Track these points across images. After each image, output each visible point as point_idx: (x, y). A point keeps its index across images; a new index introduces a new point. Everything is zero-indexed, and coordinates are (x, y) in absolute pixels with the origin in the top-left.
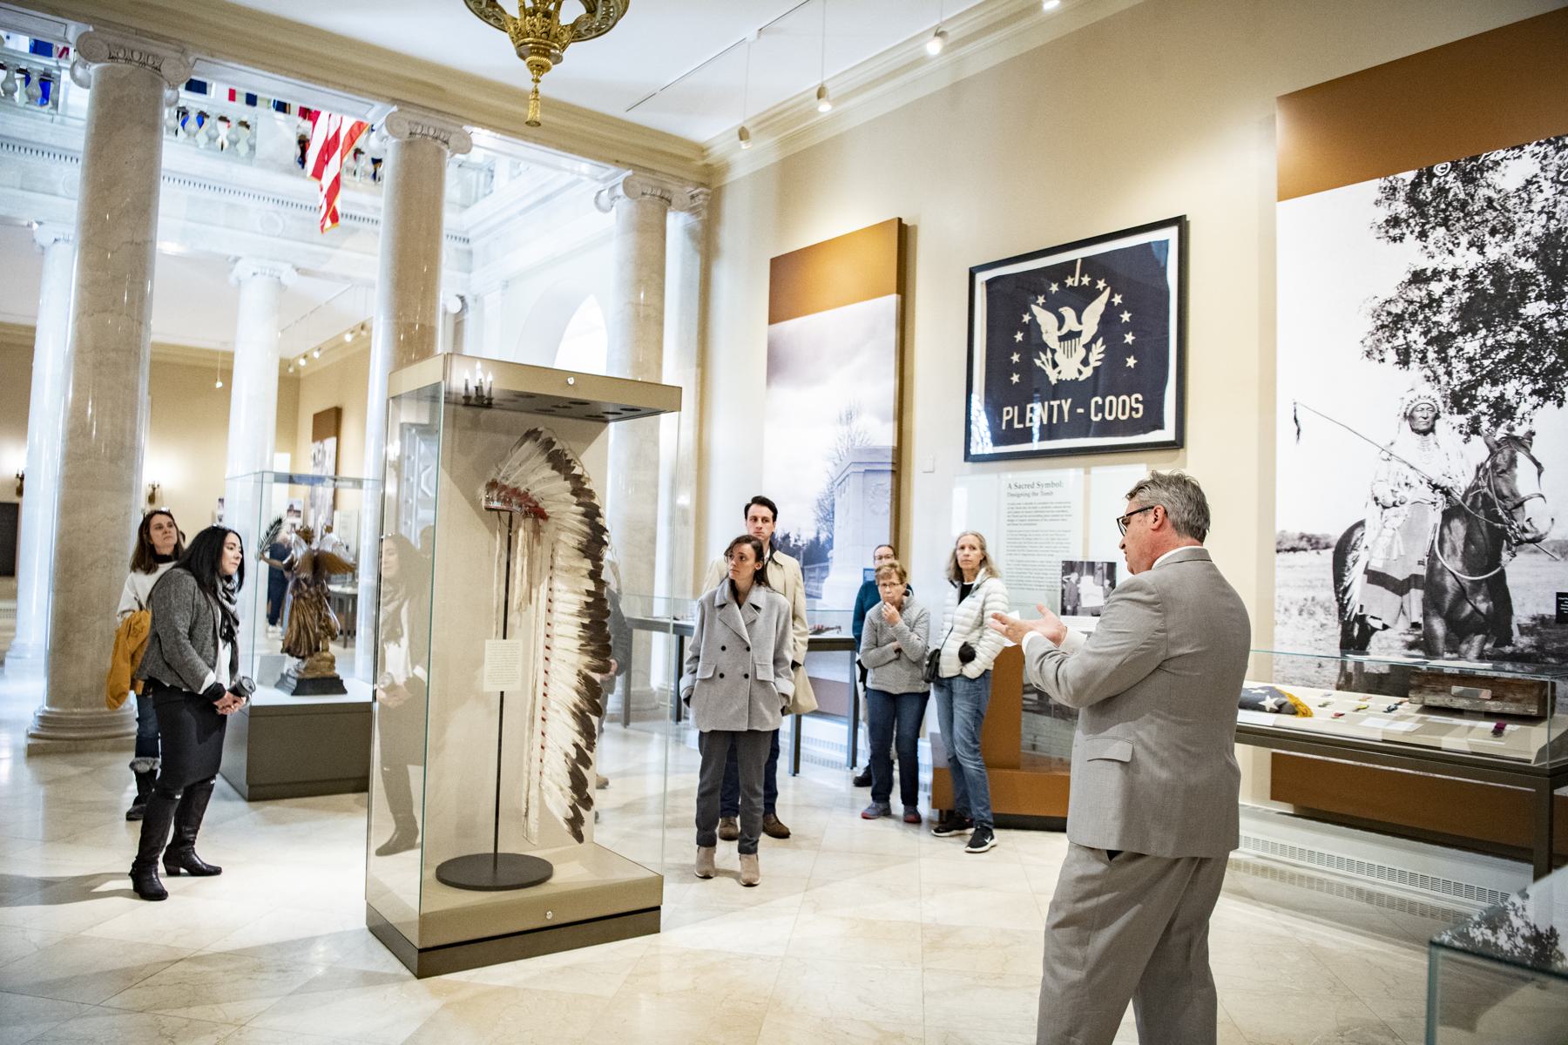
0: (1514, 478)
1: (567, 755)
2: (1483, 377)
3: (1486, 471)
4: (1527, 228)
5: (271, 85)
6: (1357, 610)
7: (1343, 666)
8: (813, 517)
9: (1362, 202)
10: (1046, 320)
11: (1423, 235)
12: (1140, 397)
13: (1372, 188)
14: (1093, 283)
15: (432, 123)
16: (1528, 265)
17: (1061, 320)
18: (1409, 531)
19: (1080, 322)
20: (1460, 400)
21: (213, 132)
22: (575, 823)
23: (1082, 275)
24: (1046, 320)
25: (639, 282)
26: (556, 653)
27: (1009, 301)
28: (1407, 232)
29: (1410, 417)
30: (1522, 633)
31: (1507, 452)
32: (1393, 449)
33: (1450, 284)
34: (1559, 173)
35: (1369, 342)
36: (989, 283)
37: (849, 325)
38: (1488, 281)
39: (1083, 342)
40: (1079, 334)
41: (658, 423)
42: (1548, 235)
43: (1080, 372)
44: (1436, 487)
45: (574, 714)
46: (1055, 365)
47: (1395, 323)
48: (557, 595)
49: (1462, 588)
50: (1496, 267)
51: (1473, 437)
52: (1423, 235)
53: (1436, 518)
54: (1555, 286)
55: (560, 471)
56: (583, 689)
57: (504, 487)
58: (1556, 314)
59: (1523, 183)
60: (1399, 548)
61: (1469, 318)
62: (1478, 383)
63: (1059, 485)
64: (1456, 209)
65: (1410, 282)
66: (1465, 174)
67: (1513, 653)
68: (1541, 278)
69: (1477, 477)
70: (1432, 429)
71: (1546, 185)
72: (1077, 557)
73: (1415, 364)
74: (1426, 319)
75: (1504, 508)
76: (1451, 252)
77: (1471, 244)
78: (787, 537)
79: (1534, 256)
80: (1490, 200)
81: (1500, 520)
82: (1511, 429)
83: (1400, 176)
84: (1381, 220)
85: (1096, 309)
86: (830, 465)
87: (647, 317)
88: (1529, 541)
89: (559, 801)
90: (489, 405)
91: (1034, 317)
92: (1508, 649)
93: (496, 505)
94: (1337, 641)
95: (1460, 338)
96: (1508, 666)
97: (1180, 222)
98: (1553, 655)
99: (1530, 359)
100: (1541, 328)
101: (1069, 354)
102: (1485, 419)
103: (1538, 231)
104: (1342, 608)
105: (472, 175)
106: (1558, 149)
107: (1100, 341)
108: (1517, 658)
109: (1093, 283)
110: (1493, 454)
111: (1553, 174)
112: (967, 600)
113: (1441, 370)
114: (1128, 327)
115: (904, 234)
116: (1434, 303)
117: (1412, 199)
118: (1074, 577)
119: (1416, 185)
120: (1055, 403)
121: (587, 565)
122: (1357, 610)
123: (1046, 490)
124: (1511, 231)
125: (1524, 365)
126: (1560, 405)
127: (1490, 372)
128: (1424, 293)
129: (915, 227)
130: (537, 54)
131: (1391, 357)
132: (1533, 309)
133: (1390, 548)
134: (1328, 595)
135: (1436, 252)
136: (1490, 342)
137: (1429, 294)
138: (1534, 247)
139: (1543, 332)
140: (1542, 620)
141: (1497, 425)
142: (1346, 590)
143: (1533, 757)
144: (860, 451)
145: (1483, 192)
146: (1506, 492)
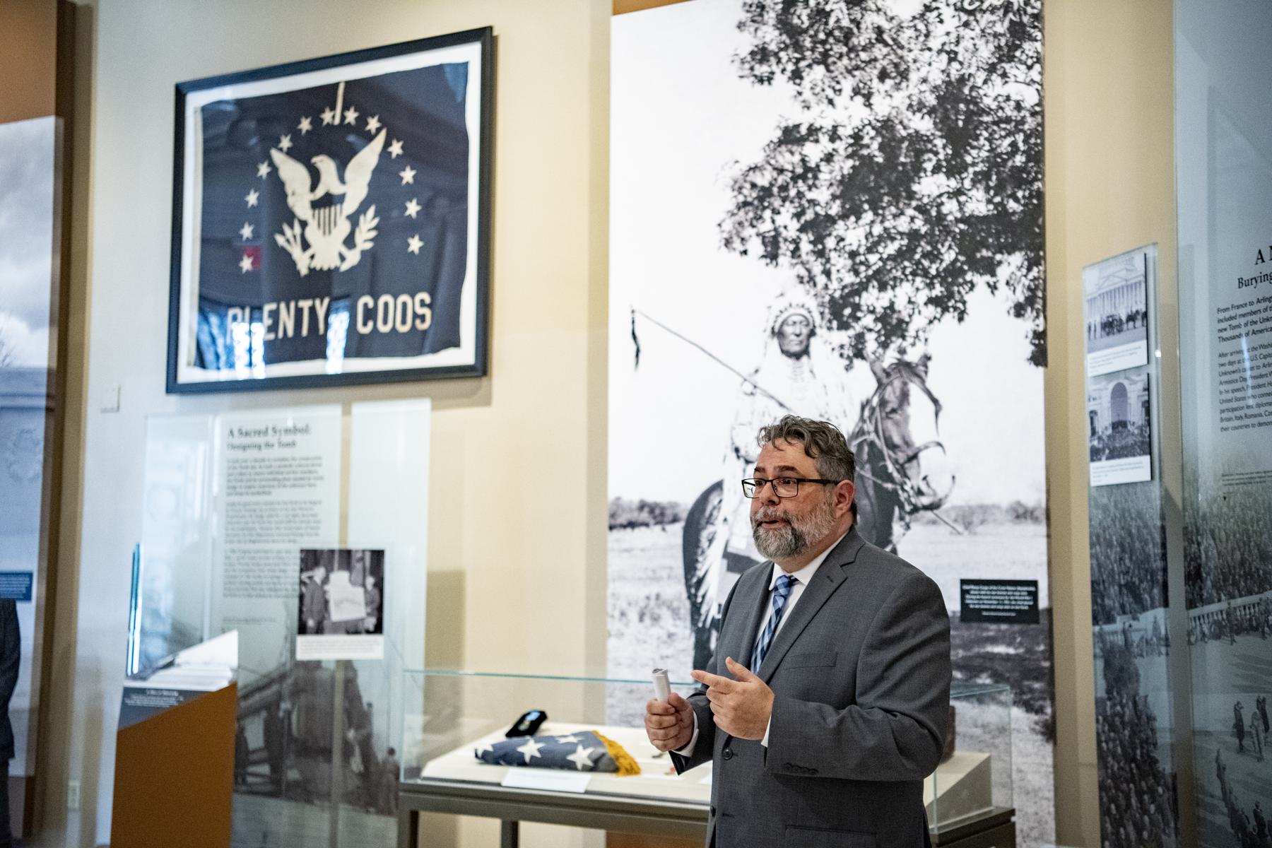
0: (906, 418)
2: (869, 279)
4: (923, 73)
10: (293, 174)
14: (362, 121)
16: (924, 125)
19: (342, 180)
20: (841, 310)
23: (346, 108)
24: (293, 174)
29: (779, 334)
31: (897, 384)
32: (758, 379)
35: (728, 226)
38: (875, 145)
42: (948, 83)
43: (342, 258)
50: (886, 127)
51: (857, 362)
52: (797, 75)
54: (957, 154)
58: (958, 193)
59: (920, 9)
62: (862, 287)
63: (305, 430)
64: (838, 41)
69: (862, 419)
70: (806, 352)
71: (948, 12)
72: (327, 540)
73: (785, 259)
74: (800, 195)
75: (896, 462)
76: (831, 102)
79: (932, 111)
80: (879, 31)
81: (890, 478)
82: (902, 351)
84: (745, 52)
85: (368, 157)
88: (926, 508)
91: (274, 170)
97: (483, 36)
98: (960, 668)
99: (924, 255)
100: (939, 212)
101: (327, 228)
102: (870, 338)
103: (937, 78)
104: (696, 609)
107: (371, 211)
109: (362, 121)
110: (881, 386)
113: (817, 268)
114: (411, 192)
116: (808, 173)
117: (784, 24)
118: (319, 574)
120: (305, 304)
123: (287, 439)
124: (904, 75)
125: (918, 263)
126: (961, 319)
127: (877, 272)
128: (797, 158)
131: (756, 247)
132: (930, 185)
134: (676, 590)
136: (877, 230)
137: (803, 161)
138: (931, 100)
139: (941, 217)
141: (885, 345)
146: (897, 440)
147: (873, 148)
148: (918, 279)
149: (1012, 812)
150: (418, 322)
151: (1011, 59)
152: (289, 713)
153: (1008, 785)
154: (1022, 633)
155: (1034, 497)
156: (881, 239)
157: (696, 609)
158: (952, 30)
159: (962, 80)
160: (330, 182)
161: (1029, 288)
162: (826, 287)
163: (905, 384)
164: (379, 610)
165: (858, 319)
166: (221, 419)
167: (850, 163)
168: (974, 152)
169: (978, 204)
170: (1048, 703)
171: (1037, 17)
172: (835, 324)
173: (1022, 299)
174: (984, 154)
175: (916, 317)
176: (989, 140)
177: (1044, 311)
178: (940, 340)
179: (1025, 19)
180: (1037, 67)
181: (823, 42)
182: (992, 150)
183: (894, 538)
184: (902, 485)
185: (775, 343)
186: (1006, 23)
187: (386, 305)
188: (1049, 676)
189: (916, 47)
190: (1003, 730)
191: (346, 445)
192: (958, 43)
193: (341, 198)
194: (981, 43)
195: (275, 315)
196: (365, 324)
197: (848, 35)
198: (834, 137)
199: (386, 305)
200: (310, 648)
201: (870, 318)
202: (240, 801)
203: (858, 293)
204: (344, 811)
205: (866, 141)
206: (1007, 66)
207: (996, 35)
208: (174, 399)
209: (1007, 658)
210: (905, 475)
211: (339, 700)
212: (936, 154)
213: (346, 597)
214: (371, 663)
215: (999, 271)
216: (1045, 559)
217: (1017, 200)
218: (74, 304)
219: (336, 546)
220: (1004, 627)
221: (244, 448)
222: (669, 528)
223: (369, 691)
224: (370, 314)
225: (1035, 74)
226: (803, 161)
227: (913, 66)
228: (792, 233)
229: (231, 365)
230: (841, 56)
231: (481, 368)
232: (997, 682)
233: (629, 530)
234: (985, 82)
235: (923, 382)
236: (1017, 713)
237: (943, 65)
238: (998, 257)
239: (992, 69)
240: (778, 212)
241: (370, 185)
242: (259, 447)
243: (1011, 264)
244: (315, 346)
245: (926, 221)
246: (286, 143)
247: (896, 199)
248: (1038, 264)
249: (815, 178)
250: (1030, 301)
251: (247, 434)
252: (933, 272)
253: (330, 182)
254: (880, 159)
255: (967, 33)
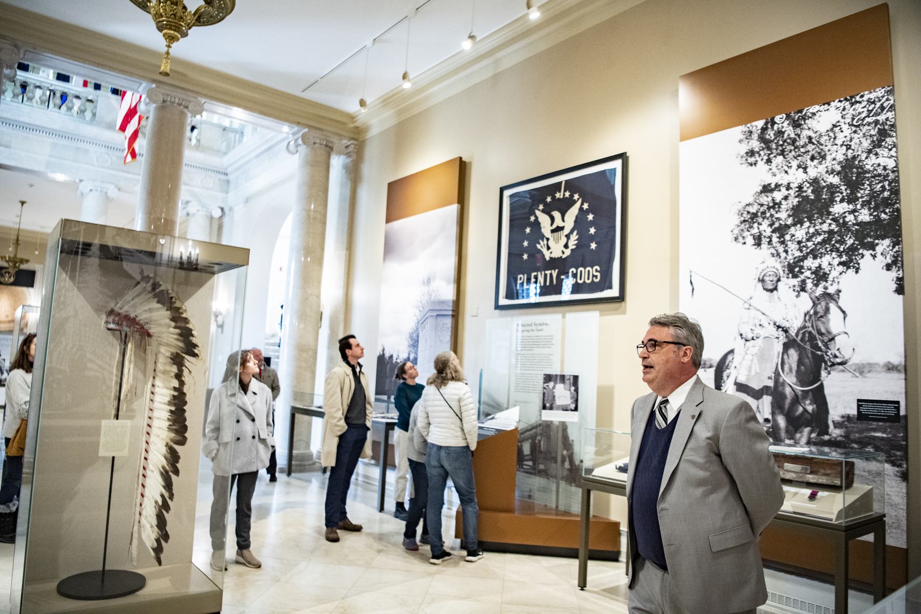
0: (828, 320)
1: (156, 502)
2: (808, 254)
3: (811, 316)
4: (833, 156)
5: (111, 79)
9: (733, 140)
10: (544, 219)
13: (738, 132)
14: (572, 196)
15: (179, 95)
16: (835, 180)
17: (553, 219)
18: (762, 357)
19: (563, 221)
20: (793, 269)
21: (70, 105)
22: (158, 550)
23: (565, 191)
24: (544, 219)
25: (309, 198)
26: (154, 431)
27: (527, 208)
28: (759, 159)
29: (762, 281)
30: (835, 427)
32: (751, 302)
33: (786, 193)
34: (853, 119)
35: (736, 231)
36: (511, 196)
37: (431, 223)
38: (810, 191)
39: (565, 235)
40: (562, 228)
42: (847, 160)
43: (563, 253)
44: (779, 327)
45: (162, 473)
46: (549, 248)
47: (752, 218)
48: (157, 390)
49: (796, 395)
50: (815, 182)
51: (802, 293)
52: (769, 161)
54: (852, 193)
55: (163, 304)
56: (168, 456)
57: (119, 314)
58: (853, 211)
59: (831, 126)
60: (756, 368)
61: (800, 214)
62: (805, 258)
63: (547, 324)
64: (789, 144)
65: (761, 192)
66: (794, 121)
67: (830, 441)
68: (843, 188)
69: (805, 321)
70: (776, 289)
71: (845, 127)
72: (555, 371)
73: (764, 246)
74: (772, 216)
75: (823, 341)
76: (786, 172)
77: (799, 167)
78: (391, 357)
79: (839, 173)
80: (810, 138)
81: (820, 349)
82: (826, 288)
83: (754, 123)
84: (743, 152)
85: (573, 212)
86: (417, 311)
87: (315, 219)
88: (839, 364)
89: (149, 534)
90: (196, 269)
91: (536, 217)
92: (826, 438)
93: (112, 326)
95: (793, 228)
96: (826, 449)
97: (623, 156)
98: (856, 442)
99: (837, 242)
100: (844, 221)
101: (557, 241)
102: (809, 282)
103: (841, 157)
105: (232, 135)
106: (852, 104)
107: (575, 232)
108: (833, 444)
109: (572, 196)
110: (815, 305)
111: (850, 120)
114: (592, 224)
115: (463, 167)
116: (776, 205)
117: (762, 139)
118: (551, 384)
119: (764, 129)
120: (548, 272)
121: (174, 369)
123: (539, 328)
124: (824, 157)
125: (834, 245)
126: (857, 272)
128: (770, 199)
129: (470, 163)
130: (170, 29)
131: (750, 241)
132: (838, 208)
133: (750, 368)
136: (812, 230)
137: (773, 200)
138: (838, 168)
139: (845, 223)
140: (848, 418)
141: (817, 285)
143: (834, 517)
145: (805, 133)
146: (823, 330)
147: (809, 192)
148: (834, 253)
149: (884, 516)
151: (880, 146)
152: (540, 441)
153: (882, 501)
154: (890, 427)
155: (897, 358)
156: (814, 235)
158: (847, 134)
159: (854, 158)
160: (558, 222)
161: (894, 256)
162: (786, 258)
163: (827, 304)
164: (577, 401)
165: (803, 273)
166: (519, 320)
167: (797, 199)
168: (862, 192)
169: (865, 216)
170: (904, 462)
171: (893, 126)
172: (790, 275)
173: (890, 262)
174: (867, 192)
175: (833, 271)
176: (870, 185)
177: (902, 266)
178: (846, 283)
179: (886, 127)
180: (894, 149)
181: (782, 145)
182: (871, 190)
183: (822, 378)
184: (826, 352)
186: (876, 130)
188: (905, 449)
189: (829, 144)
190: (879, 474)
191: (563, 330)
192: (851, 141)
194: (863, 140)
198: (788, 187)
200: (547, 416)
201: (809, 272)
202: (520, 476)
203: (802, 260)
204: (563, 484)
205: (805, 189)
206: (878, 150)
207: (871, 136)
208: (498, 311)
209: (882, 439)
211: (560, 435)
212: (842, 193)
213: (562, 394)
214: (573, 423)
215: (877, 248)
216: (903, 390)
217: (886, 213)
218: (462, 276)
219: (559, 373)
220: (881, 424)
222: (708, 370)
223: (572, 435)
225: (893, 153)
226: (773, 200)
227: (828, 153)
228: (768, 233)
229: (528, 296)
230: (791, 151)
231: (621, 298)
232: (876, 451)
234: (866, 158)
235: (837, 302)
236: (887, 466)
237: (844, 151)
238: (877, 241)
239: (869, 152)
240: (760, 224)
243: (884, 245)
244: (558, 290)
245: (837, 226)
246: (541, 207)
247: (821, 216)
248: (898, 244)
249: (779, 207)
250: (895, 262)
252: (842, 249)
253: (558, 222)
255: (856, 136)
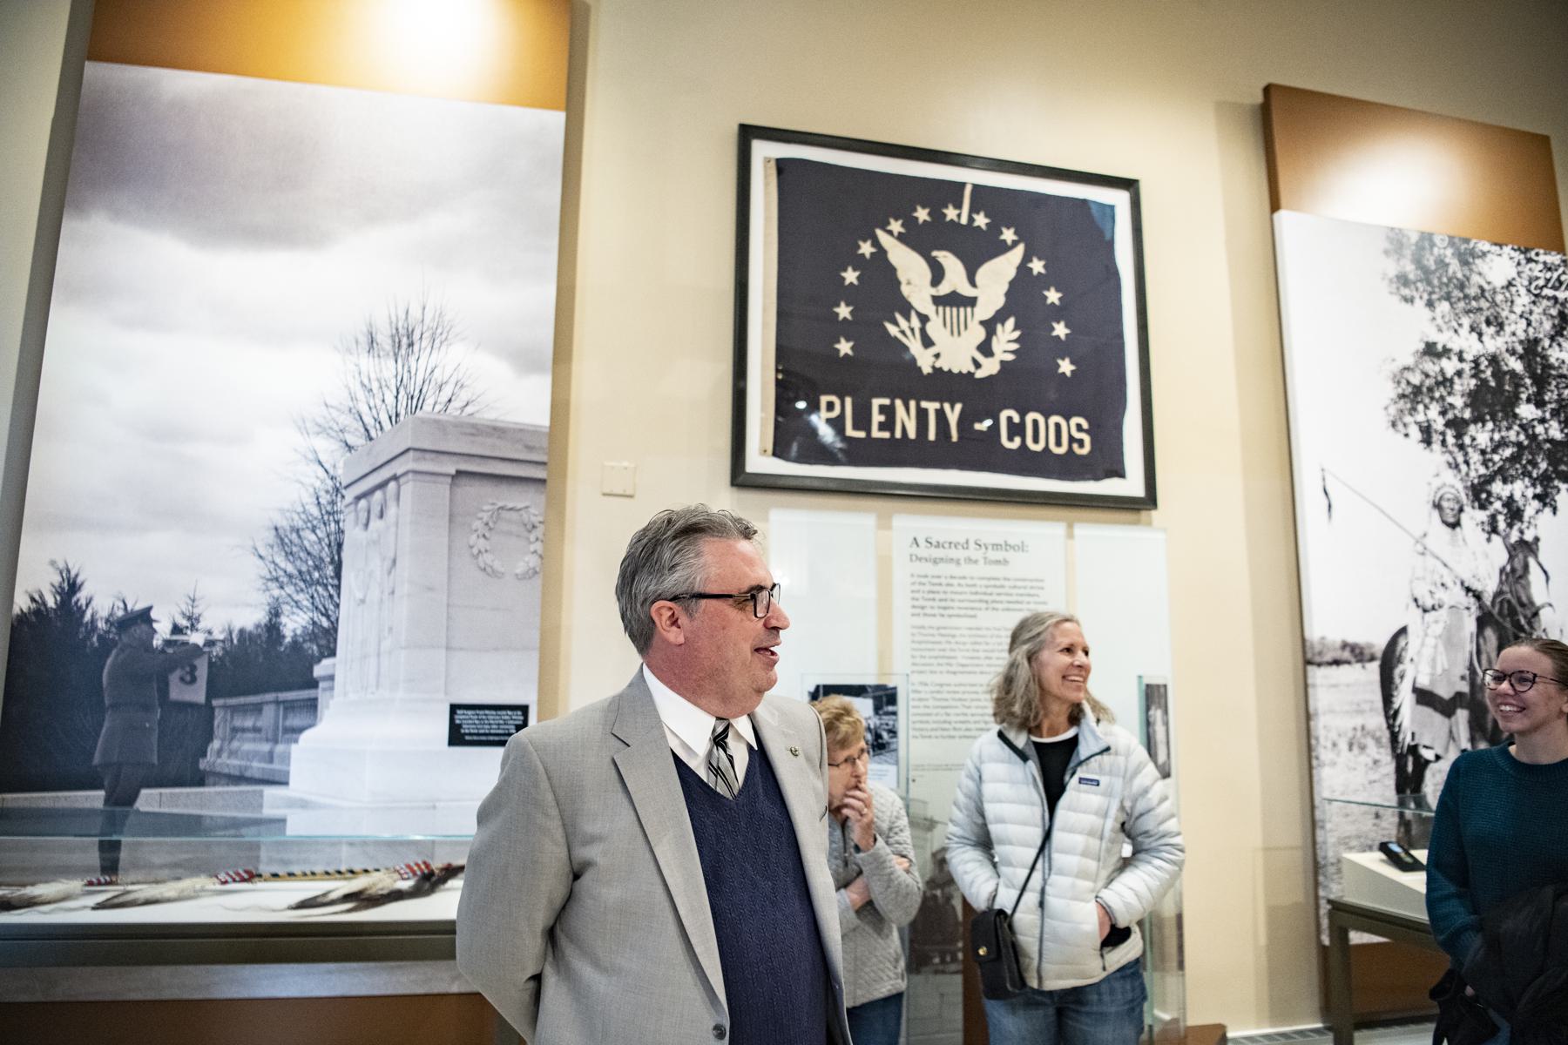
0: (1529, 583)
4: (1513, 327)
6: (1408, 740)
7: (1401, 815)
8: (257, 569)
10: (909, 266)
11: (1430, 304)
12: (1085, 425)
16: (1516, 365)
17: (938, 274)
18: (1449, 640)
19: (973, 283)
23: (974, 209)
24: (909, 266)
28: (1417, 296)
29: (1438, 506)
31: (1521, 556)
32: (1427, 541)
35: (1393, 410)
41: (557, 108)
43: (978, 365)
44: (1468, 590)
46: (927, 342)
50: (1494, 360)
51: (1494, 536)
53: (1470, 626)
58: (1542, 421)
62: (1489, 480)
63: (1021, 547)
69: (1501, 582)
73: (1436, 446)
79: (1521, 357)
82: (1522, 532)
94: (1391, 782)
101: (957, 330)
102: (1501, 518)
104: (1394, 737)
107: (1011, 322)
109: (994, 228)
110: (1511, 558)
112: (1074, 795)
113: (1460, 459)
114: (1058, 313)
120: (931, 407)
122: (1408, 740)
123: (999, 555)
127: (1500, 468)
128: (1437, 369)
133: (1434, 660)
134: (1378, 721)
135: (1444, 327)
136: (1497, 437)
138: (1520, 349)
141: (1510, 526)
142: (1397, 712)
144: (439, 426)
146: (1524, 599)
150: (1075, 446)
157: (1394, 737)
185: (1436, 513)
187: (1035, 422)
193: (972, 302)
195: (888, 411)
196: (1011, 439)
197: (1462, 287)
199: (1035, 422)
210: (1532, 627)
221: (935, 561)
222: (1368, 665)
224: (1016, 430)
231: (1150, 500)
233: (1334, 667)
241: (1008, 295)
242: (958, 562)
251: (938, 545)
254: (1493, 384)
